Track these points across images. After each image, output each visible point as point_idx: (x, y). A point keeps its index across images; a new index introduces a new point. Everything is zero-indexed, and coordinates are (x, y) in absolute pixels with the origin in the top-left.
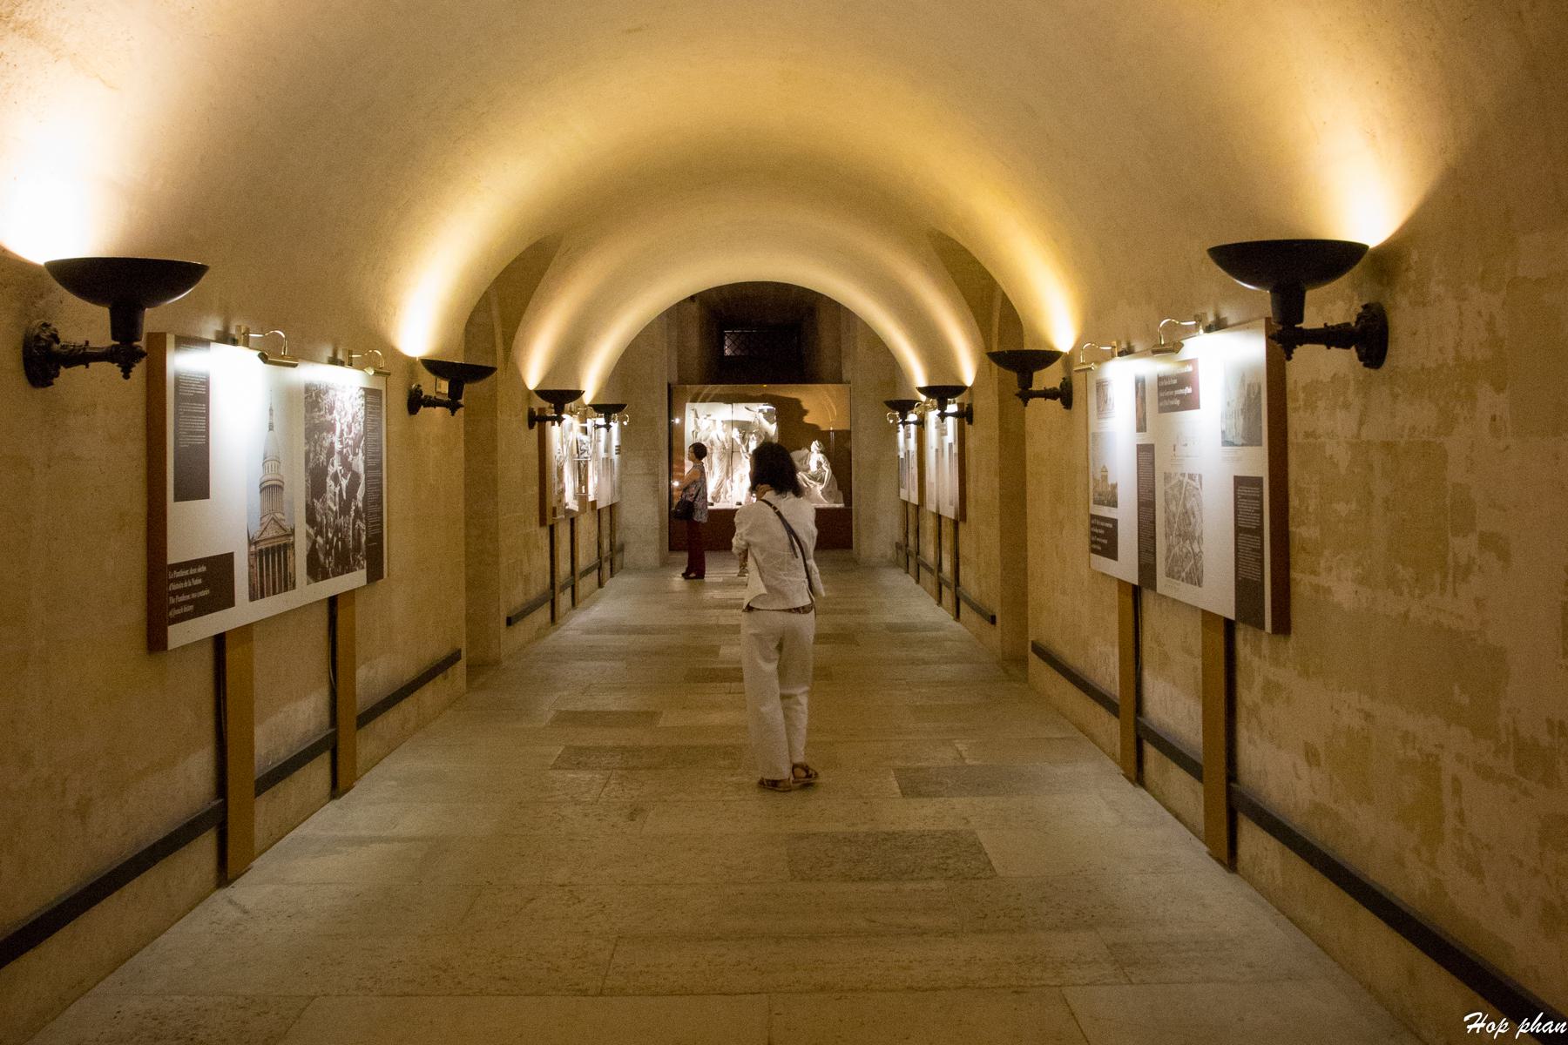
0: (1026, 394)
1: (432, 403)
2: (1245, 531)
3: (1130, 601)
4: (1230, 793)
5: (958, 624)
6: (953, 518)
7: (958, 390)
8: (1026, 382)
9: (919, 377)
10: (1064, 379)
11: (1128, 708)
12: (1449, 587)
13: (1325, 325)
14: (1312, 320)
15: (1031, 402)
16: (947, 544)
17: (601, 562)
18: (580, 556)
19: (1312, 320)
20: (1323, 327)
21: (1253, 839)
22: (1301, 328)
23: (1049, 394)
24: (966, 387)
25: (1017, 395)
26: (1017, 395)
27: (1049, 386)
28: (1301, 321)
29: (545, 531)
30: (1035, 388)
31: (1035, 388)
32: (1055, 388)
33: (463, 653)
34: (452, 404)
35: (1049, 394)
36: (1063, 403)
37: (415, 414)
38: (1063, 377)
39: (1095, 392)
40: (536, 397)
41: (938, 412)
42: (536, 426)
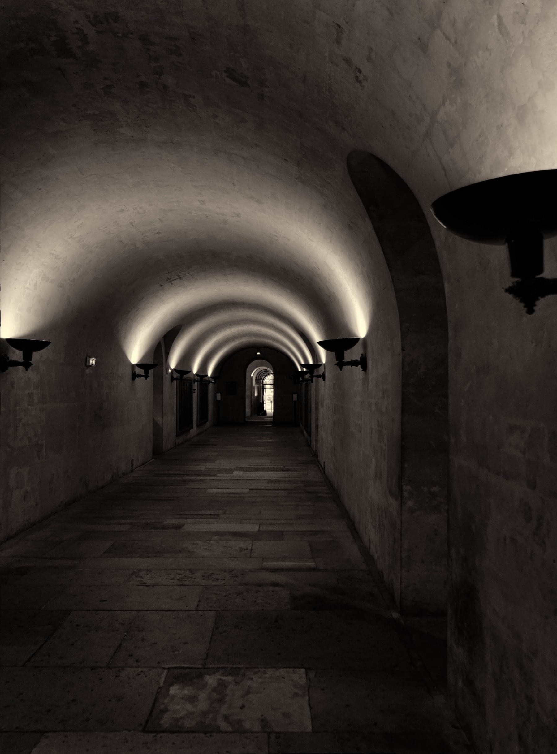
1: (140, 376)
10: (362, 354)
12: (194, 390)
13: (351, 360)
14: (347, 358)
19: (347, 358)
20: (350, 361)
22: (344, 362)
23: (354, 363)
24: (358, 339)
27: (354, 359)
28: (344, 359)
30: (314, 375)
31: (314, 375)
32: (357, 360)
34: (146, 376)
35: (354, 363)
36: (323, 379)
37: (134, 380)
38: (361, 353)
39: (253, 401)
40: (136, 366)
42: (134, 371)
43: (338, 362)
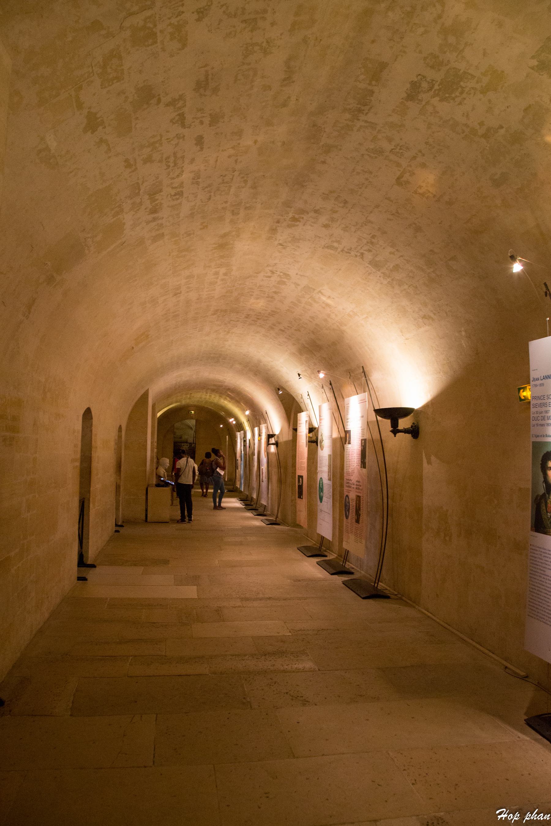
43: (392, 429)
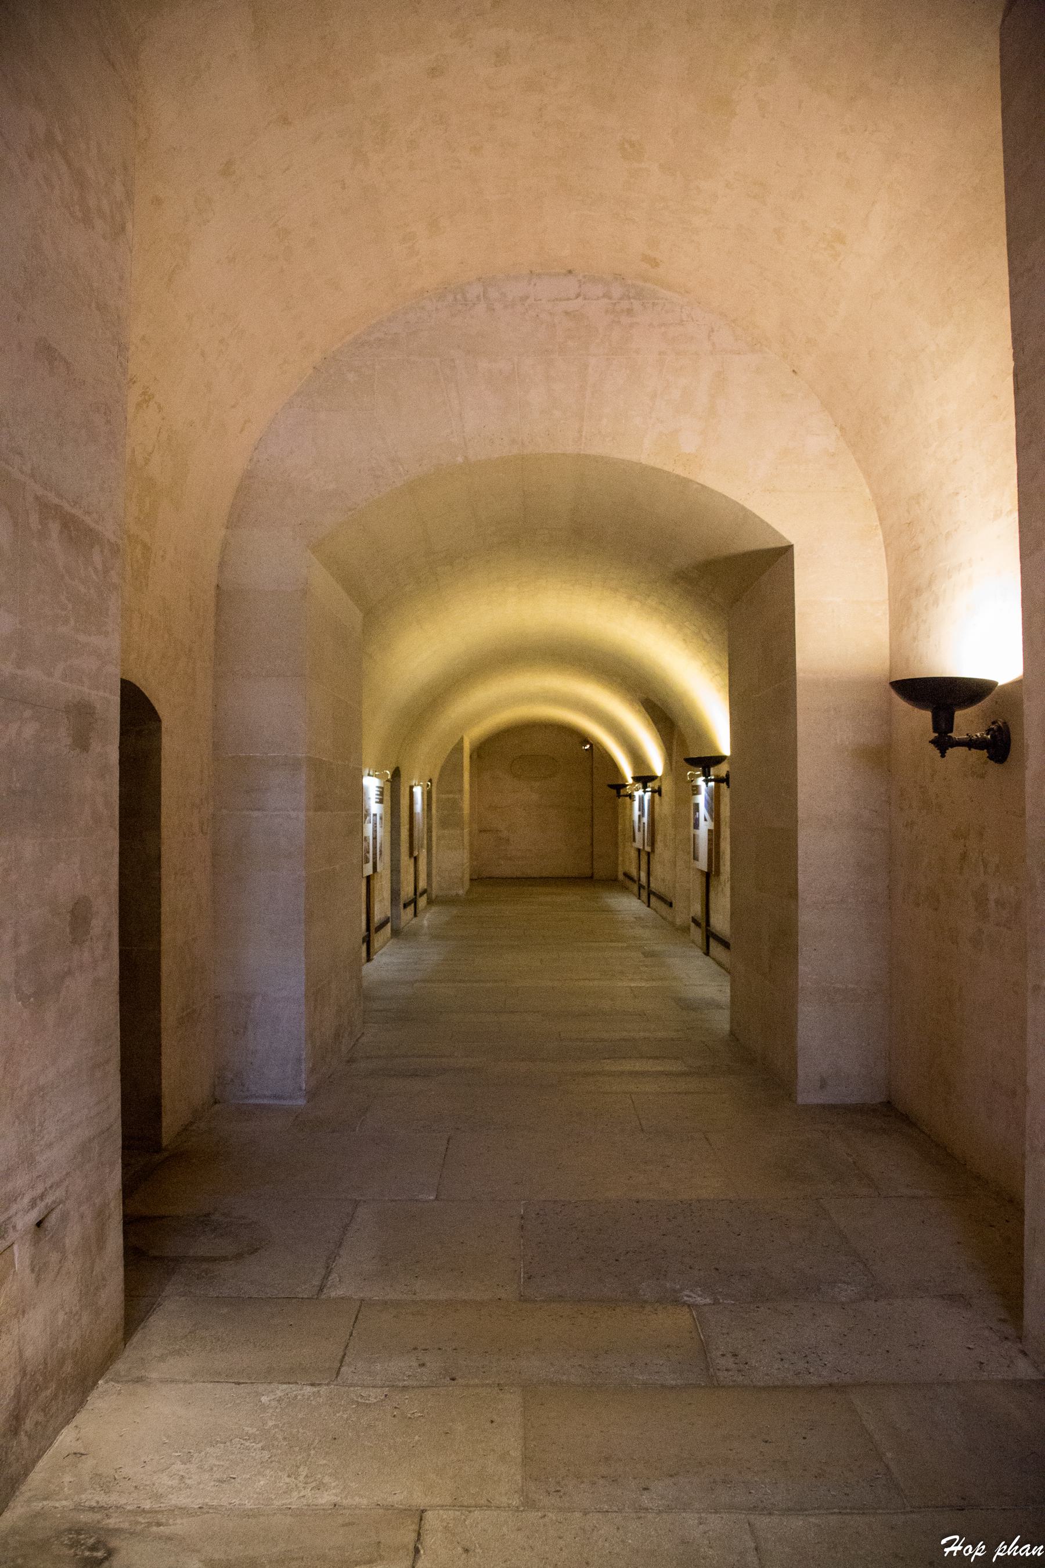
0: (619, 796)
2: (710, 840)
3: (704, 879)
4: (707, 931)
5: (648, 908)
6: (706, 870)
7: (653, 778)
8: (618, 792)
9: (628, 771)
11: (704, 924)
15: (950, 751)
16: (644, 866)
17: (416, 898)
18: (376, 909)
21: (653, 899)
25: (932, 742)
26: (932, 742)
29: (413, 860)
33: (402, 906)
41: (643, 790)
